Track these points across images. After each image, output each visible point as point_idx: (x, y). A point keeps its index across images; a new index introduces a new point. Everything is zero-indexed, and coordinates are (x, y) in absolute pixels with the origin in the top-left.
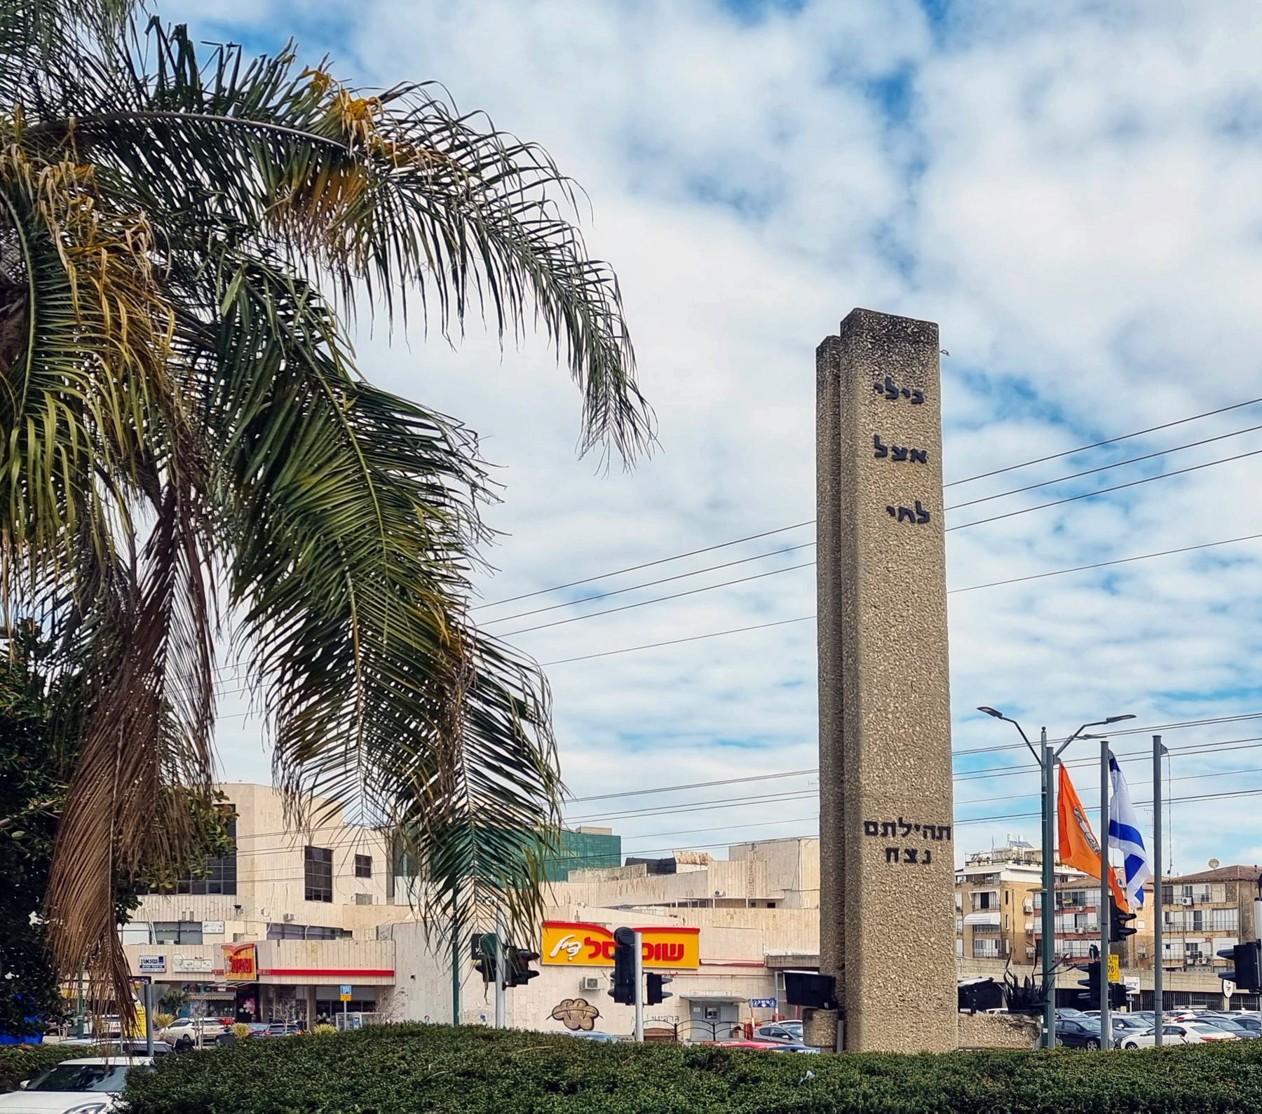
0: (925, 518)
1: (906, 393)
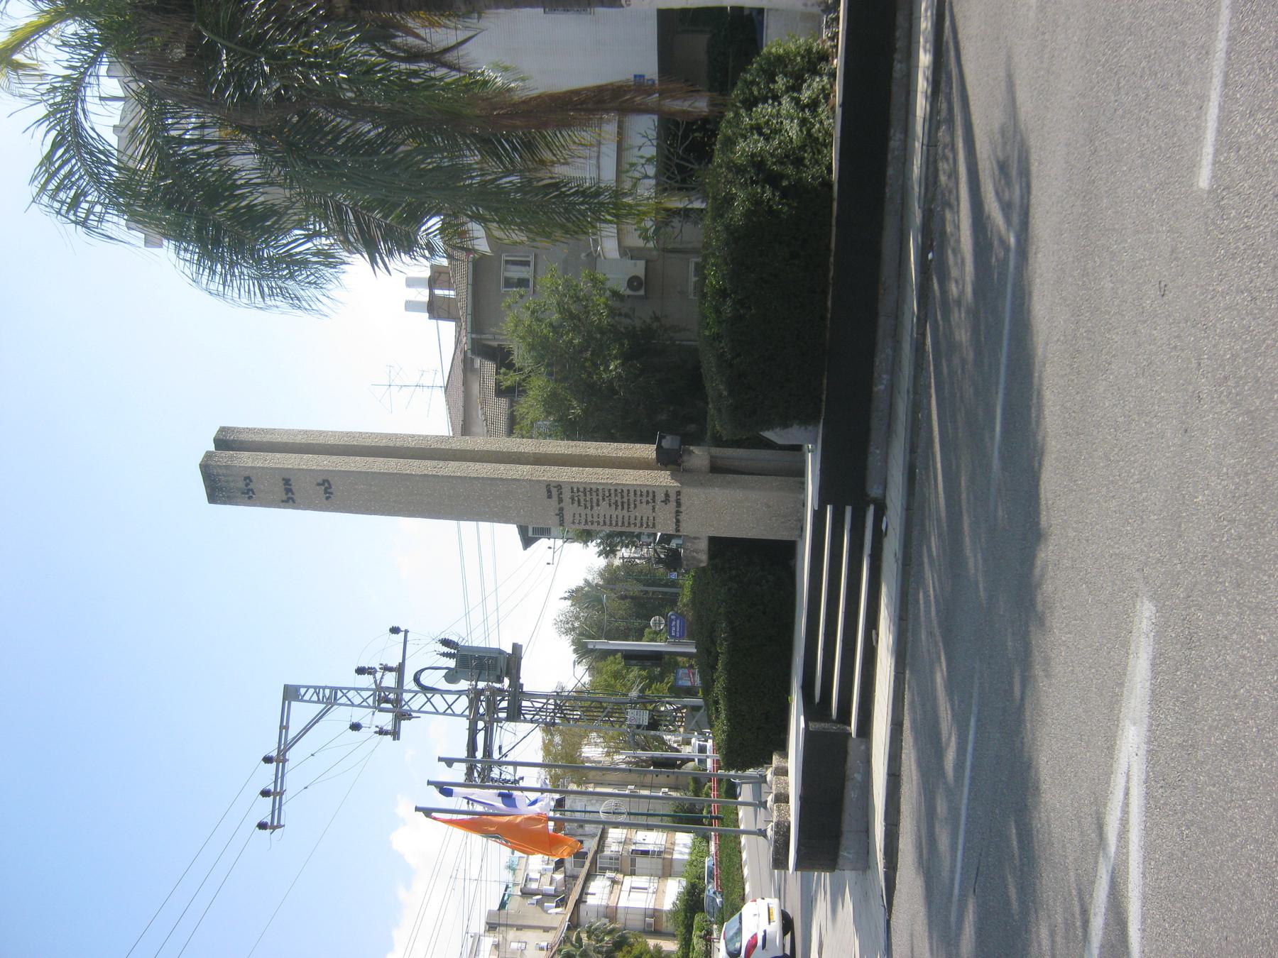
0: (325, 481)
1: (247, 485)
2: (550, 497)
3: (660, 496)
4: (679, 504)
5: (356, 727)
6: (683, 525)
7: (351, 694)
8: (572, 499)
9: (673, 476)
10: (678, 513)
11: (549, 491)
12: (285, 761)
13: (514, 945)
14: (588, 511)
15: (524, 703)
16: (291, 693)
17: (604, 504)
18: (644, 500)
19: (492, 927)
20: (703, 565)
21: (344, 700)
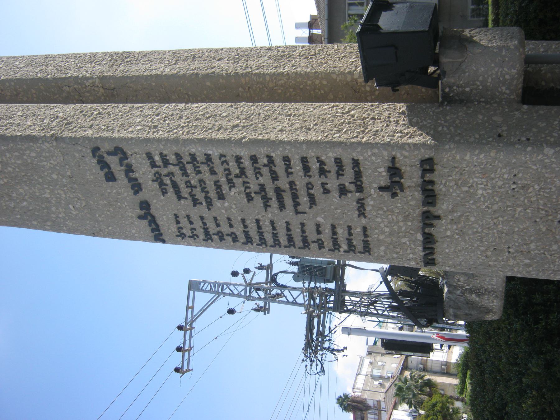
2: (110, 177)
3: (376, 175)
4: (429, 195)
5: (231, 311)
6: (442, 250)
7: (232, 287)
8: (158, 179)
9: (415, 118)
10: (428, 219)
11: (103, 164)
12: (191, 328)
13: (380, 363)
14: (202, 209)
15: (347, 298)
16: (194, 286)
17: (235, 194)
18: (333, 183)
19: (370, 353)
20: (489, 317)
21: (227, 291)
